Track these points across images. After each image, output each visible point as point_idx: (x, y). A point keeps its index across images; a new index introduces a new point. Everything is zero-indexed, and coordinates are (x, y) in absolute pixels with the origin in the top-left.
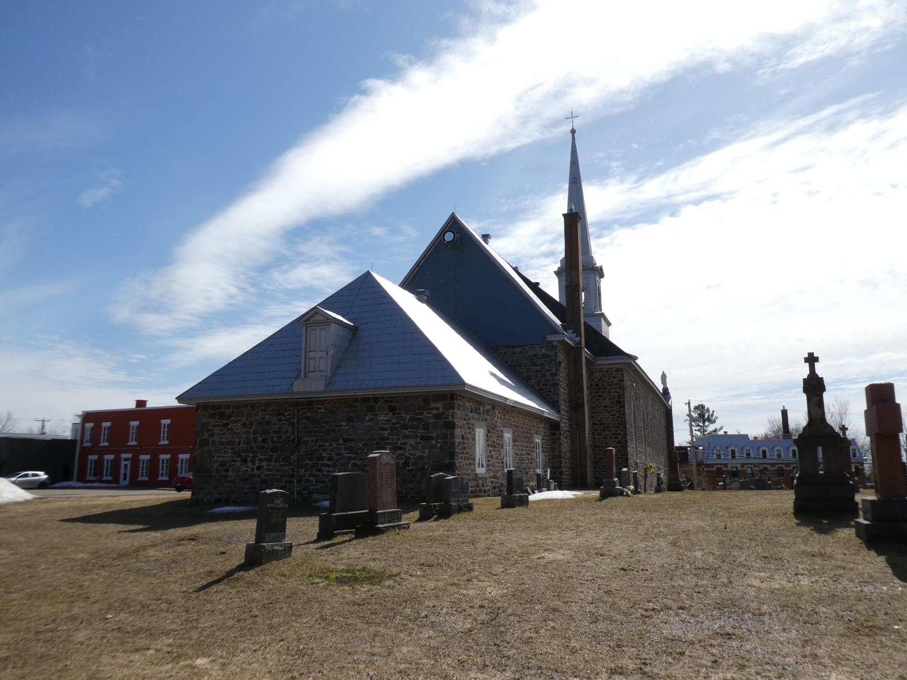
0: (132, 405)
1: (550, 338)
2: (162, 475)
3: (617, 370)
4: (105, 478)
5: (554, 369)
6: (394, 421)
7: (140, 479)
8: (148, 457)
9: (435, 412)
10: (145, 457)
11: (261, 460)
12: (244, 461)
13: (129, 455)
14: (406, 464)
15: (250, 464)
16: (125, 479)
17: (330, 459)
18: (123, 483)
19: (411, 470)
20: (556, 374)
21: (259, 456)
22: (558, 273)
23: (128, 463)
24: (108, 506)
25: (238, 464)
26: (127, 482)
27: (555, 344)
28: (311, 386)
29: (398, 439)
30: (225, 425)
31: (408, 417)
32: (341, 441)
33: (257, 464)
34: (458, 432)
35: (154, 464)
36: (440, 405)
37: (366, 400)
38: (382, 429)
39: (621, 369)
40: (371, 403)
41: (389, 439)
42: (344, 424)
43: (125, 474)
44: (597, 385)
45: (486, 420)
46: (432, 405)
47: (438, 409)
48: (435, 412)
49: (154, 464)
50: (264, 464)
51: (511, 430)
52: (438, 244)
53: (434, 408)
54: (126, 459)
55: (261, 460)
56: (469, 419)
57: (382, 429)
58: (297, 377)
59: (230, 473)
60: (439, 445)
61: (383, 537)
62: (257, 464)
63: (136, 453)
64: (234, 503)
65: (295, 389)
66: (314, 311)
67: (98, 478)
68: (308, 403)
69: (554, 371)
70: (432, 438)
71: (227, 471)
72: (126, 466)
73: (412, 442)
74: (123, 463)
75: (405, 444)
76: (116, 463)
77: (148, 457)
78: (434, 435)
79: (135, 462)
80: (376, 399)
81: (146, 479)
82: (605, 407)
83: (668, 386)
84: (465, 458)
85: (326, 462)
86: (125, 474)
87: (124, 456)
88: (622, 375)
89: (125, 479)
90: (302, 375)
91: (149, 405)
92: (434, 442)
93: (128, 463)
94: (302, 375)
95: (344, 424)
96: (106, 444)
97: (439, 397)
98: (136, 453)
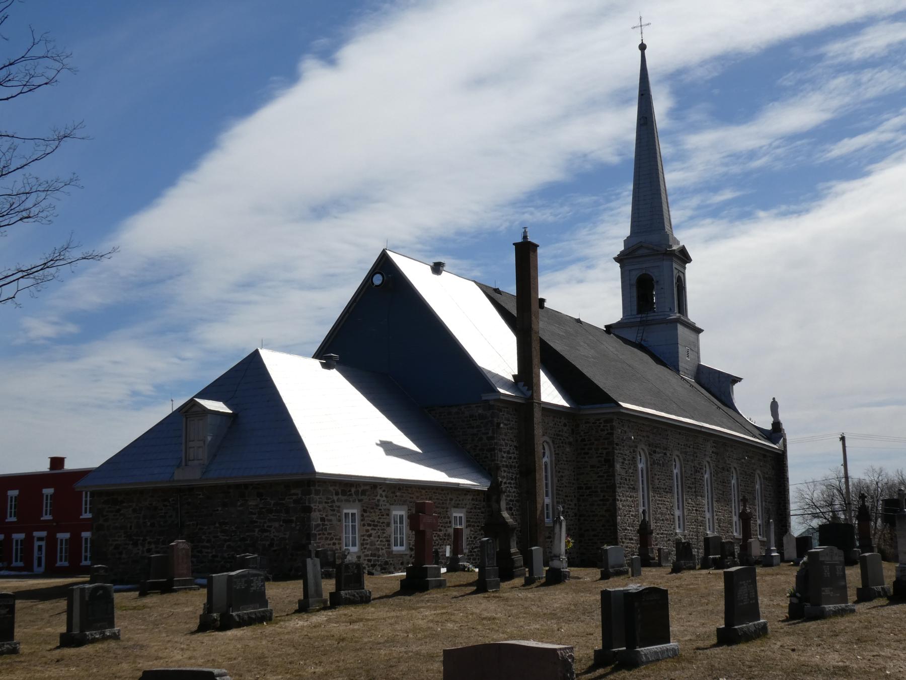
0: (44, 467)
1: (485, 397)
2: (86, 560)
3: (606, 421)
4: (14, 564)
5: (490, 432)
6: (261, 506)
7: (59, 564)
8: (67, 535)
9: (294, 497)
10: (64, 536)
11: (150, 543)
12: (135, 544)
13: (43, 534)
14: (271, 545)
15: (140, 547)
16: (39, 565)
17: (209, 541)
18: (37, 570)
19: (275, 551)
20: (492, 438)
21: (149, 539)
22: (620, 259)
23: (43, 543)
24: (17, 588)
25: (130, 547)
26: (42, 569)
27: (491, 403)
28: (190, 475)
29: (265, 523)
30: (119, 510)
31: (273, 502)
32: (217, 525)
33: (147, 546)
34: (315, 515)
35: (75, 543)
36: (299, 491)
37: (238, 486)
38: (252, 513)
39: (611, 421)
40: (242, 489)
41: (256, 522)
42: (220, 509)
43: (40, 559)
44: (583, 440)
45: (360, 501)
46: (293, 491)
47: (297, 494)
48: (294, 497)
49: (75, 543)
50: (153, 546)
51: (406, 507)
52: (366, 287)
53: (294, 494)
54: (40, 539)
55: (150, 543)
56: (333, 501)
57: (252, 513)
58: (179, 466)
59: (124, 556)
60: (298, 528)
61: (174, 594)
62: (147, 546)
63: (52, 529)
64: (127, 583)
65: (176, 478)
66: (191, 404)
67: (5, 564)
68: (189, 490)
69: (490, 434)
70: (291, 521)
71: (121, 553)
72: (40, 547)
73: (276, 524)
74: (37, 544)
75: (271, 527)
76: (28, 543)
77: (67, 535)
78: (294, 518)
79: (51, 541)
80: (246, 486)
81: (66, 564)
82: (592, 467)
83: (782, 417)
84: (327, 539)
85: (205, 544)
86: (40, 559)
87: (37, 534)
88: (612, 428)
89: (39, 565)
90: (183, 464)
91: (69, 466)
92: (293, 525)
93: (43, 543)
94: (183, 464)
95: (220, 509)
96: (14, 519)
97: (298, 484)
98: (52, 529)
